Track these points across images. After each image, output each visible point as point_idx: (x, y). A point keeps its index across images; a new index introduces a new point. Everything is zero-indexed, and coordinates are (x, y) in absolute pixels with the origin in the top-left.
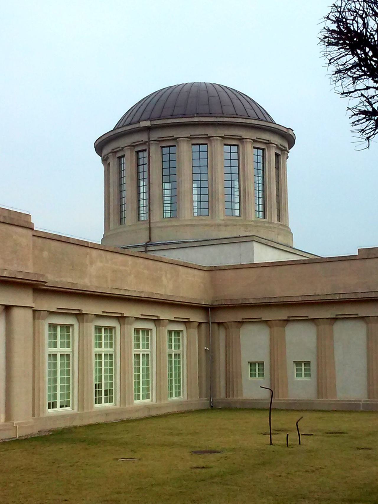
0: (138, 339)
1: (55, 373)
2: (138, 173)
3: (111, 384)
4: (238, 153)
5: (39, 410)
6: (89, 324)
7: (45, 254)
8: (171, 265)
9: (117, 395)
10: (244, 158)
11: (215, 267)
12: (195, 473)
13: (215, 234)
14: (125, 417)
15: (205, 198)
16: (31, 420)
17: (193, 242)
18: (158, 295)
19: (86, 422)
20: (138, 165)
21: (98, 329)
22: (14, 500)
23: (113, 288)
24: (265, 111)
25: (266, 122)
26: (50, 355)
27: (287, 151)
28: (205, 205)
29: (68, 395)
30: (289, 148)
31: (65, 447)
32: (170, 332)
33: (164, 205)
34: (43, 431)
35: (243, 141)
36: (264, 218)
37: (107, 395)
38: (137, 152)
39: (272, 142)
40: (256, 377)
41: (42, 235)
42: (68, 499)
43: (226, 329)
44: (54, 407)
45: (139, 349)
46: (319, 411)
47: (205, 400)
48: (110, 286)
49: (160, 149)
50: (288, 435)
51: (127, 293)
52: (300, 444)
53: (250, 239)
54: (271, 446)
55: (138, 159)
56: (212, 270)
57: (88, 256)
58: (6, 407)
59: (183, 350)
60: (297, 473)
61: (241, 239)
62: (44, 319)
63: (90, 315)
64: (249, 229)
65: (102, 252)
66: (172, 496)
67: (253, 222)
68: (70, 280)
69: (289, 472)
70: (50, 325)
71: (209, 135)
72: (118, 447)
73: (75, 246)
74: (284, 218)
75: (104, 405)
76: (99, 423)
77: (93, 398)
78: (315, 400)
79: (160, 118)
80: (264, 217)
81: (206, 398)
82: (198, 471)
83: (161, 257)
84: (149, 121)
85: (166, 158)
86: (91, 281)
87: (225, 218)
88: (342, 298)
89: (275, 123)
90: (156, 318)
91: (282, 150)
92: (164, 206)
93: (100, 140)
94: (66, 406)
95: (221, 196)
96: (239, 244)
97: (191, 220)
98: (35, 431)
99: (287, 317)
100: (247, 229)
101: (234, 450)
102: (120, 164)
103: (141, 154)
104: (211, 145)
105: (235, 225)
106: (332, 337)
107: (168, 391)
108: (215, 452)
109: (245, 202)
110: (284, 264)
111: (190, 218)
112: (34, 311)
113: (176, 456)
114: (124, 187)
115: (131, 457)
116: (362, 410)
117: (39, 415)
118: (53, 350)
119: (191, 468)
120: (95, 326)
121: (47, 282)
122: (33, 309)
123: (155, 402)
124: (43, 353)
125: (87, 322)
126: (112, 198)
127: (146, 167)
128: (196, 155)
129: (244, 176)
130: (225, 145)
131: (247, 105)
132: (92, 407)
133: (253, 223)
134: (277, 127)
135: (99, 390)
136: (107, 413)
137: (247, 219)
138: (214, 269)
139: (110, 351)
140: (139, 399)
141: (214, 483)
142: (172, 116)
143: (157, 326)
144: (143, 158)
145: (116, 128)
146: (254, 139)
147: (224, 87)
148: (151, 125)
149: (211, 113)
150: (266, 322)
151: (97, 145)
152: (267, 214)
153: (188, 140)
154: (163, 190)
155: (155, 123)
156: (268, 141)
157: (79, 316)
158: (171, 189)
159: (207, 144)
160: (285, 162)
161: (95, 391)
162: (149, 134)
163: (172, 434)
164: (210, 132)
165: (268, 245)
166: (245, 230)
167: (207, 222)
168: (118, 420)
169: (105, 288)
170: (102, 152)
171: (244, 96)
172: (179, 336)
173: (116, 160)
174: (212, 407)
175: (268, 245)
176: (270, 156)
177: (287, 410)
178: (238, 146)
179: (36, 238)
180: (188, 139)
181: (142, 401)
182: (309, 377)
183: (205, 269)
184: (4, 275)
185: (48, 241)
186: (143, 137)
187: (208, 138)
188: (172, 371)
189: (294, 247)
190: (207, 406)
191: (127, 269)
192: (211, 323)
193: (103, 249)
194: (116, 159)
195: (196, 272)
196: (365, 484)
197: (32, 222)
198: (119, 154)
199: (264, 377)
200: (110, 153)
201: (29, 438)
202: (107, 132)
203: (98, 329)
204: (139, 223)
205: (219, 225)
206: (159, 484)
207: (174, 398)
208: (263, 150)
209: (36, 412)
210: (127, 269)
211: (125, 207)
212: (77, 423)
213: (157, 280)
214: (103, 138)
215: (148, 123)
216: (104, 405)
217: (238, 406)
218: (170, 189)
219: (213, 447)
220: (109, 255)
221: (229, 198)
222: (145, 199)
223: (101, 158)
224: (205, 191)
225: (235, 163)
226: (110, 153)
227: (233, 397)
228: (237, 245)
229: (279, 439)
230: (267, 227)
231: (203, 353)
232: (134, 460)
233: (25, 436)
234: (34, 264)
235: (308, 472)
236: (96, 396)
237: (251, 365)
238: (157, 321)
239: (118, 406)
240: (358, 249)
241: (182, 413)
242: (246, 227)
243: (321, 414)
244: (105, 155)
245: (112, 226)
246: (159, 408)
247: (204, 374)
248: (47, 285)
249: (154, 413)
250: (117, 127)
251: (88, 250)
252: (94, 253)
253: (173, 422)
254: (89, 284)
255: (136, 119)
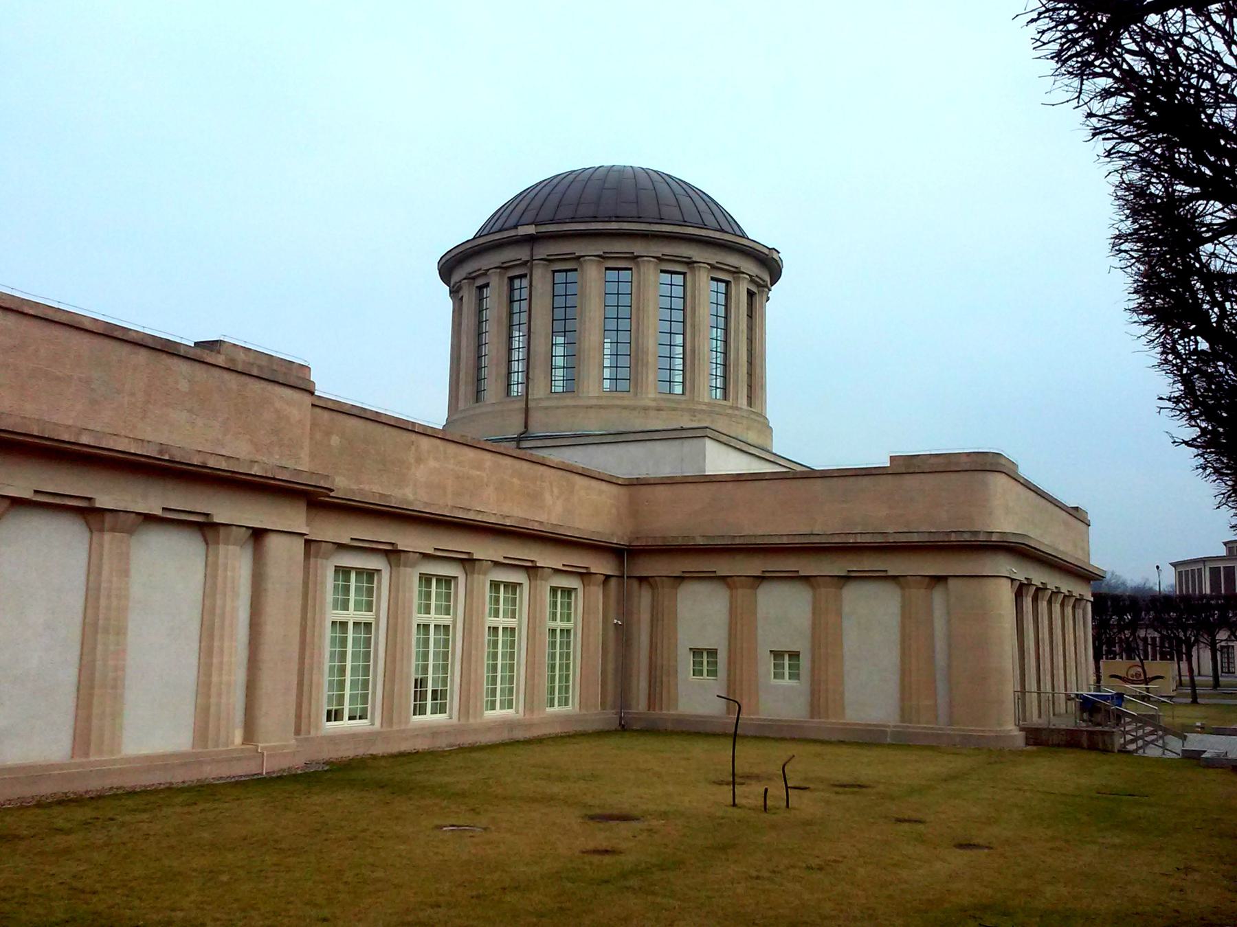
0: (497, 600)
1: (343, 656)
2: (511, 314)
3: (445, 681)
4: (683, 286)
5: (309, 725)
6: (409, 570)
7: (335, 440)
8: (560, 473)
9: (453, 701)
10: (694, 297)
11: (637, 478)
12: (591, 864)
13: (638, 423)
14: (468, 740)
15: (625, 361)
16: (293, 742)
17: (601, 435)
18: (536, 524)
19: (395, 748)
20: (511, 301)
21: (426, 579)
22: (218, 915)
23: (455, 507)
24: (731, 217)
25: (734, 236)
26: (334, 623)
27: (766, 286)
28: (623, 373)
29: (365, 698)
30: (771, 281)
31: (346, 798)
32: (554, 590)
33: (553, 382)
34: (314, 763)
35: (694, 267)
36: (725, 400)
37: (437, 700)
38: (511, 279)
39: (742, 270)
40: (702, 675)
41: (330, 405)
42: (329, 916)
43: (651, 586)
44: (338, 718)
45: (497, 619)
46: (815, 741)
47: (611, 714)
48: (450, 503)
49: (549, 275)
50: (766, 790)
51: (479, 518)
52: (788, 806)
53: (699, 433)
54: (735, 808)
55: (512, 289)
56: (633, 484)
57: (413, 448)
58: (245, 715)
59: (576, 624)
60: (792, 871)
61: (684, 434)
62: (326, 556)
63: (411, 554)
64: (699, 416)
65: (438, 441)
66: (542, 917)
67: (705, 405)
68: (377, 489)
69: (776, 869)
70: (338, 569)
71: (635, 254)
72: (445, 802)
73: (390, 429)
74: (758, 402)
75: (429, 718)
76: (417, 752)
77: (410, 706)
78: (806, 722)
79: (552, 222)
80: (725, 397)
81: (612, 709)
82: (596, 859)
83: (544, 457)
84: (534, 226)
85: (560, 289)
86: (415, 494)
87: (659, 396)
88: (859, 541)
89: (748, 238)
90: (529, 564)
91: (759, 285)
92: (553, 384)
93: (448, 257)
94: (361, 718)
95: (651, 359)
96: (680, 441)
97: (598, 398)
98: (297, 763)
99: (760, 571)
100: (695, 416)
101: (664, 815)
102: (481, 300)
103: (517, 283)
104: (639, 272)
105: (674, 409)
106: (839, 613)
107: (547, 696)
108: (625, 818)
109: (693, 371)
110: (760, 477)
111: (597, 395)
112: (308, 542)
113: (554, 824)
114: (486, 338)
115: (468, 822)
116: (891, 742)
117: (309, 732)
118: (340, 615)
119: (583, 852)
120: (420, 574)
121: (335, 489)
122: (306, 537)
123: (522, 714)
124: (322, 620)
125: (405, 566)
126: (464, 353)
127: (525, 304)
128: (612, 288)
129: (693, 326)
130: (662, 271)
131: (702, 206)
132: (408, 721)
133: (704, 407)
134: (751, 244)
135: (422, 689)
136: (435, 732)
137: (696, 399)
138: (635, 483)
139: (445, 620)
140: (494, 709)
141: (627, 888)
142: (573, 220)
143: (531, 578)
144: (521, 288)
145: (477, 236)
146: (659, 257)
147: (664, 176)
148: (537, 233)
149: (641, 216)
150: (723, 579)
151: (442, 265)
152: (729, 392)
153: (599, 261)
154: (552, 356)
155: (543, 229)
156: (736, 268)
157: (392, 554)
158: (566, 368)
159: (631, 269)
160: (763, 307)
161: (415, 691)
162: (532, 249)
163: (549, 778)
164: (638, 248)
165: (731, 446)
166: (692, 418)
167: (626, 403)
168: (454, 746)
169: (443, 506)
170: (450, 279)
171: (697, 190)
172: (569, 597)
173: (474, 291)
174: (624, 728)
175: (731, 446)
176: (738, 294)
177: (756, 738)
178: (684, 274)
179: (318, 410)
180: (601, 260)
181: (499, 713)
182: (796, 679)
183: (620, 483)
184: (253, 473)
185: (341, 417)
186: (522, 254)
187: (634, 258)
188: (555, 660)
189: (774, 451)
190: (615, 725)
191: (484, 475)
192: (627, 577)
193: (440, 436)
194: (474, 291)
195: (604, 486)
196: (929, 901)
197: (312, 379)
198: (480, 282)
199: (716, 676)
200: (465, 279)
201: (285, 776)
202: (460, 243)
203: (426, 579)
204: (508, 399)
205: (646, 409)
206: (517, 888)
207: (557, 709)
208: (727, 283)
209: (304, 728)
210: (484, 475)
211: (485, 372)
212: (379, 749)
213: (535, 497)
214: (453, 254)
215: (531, 230)
216: (429, 718)
217: (670, 726)
218: (564, 356)
219: (626, 808)
220: (452, 448)
221: (665, 363)
222: (521, 383)
223: (448, 288)
224: (624, 349)
225: (678, 303)
226: (465, 279)
227: (661, 709)
228: (677, 442)
229: (750, 794)
230: (729, 416)
231: (611, 633)
232: (475, 830)
233: (279, 771)
234: (313, 456)
235: (812, 869)
236: (415, 700)
237: (694, 652)
238: (532, 570)
239: (455, 720)
240: (891, 457)
241: (569, 736)
242: (693, 412)
243: (817, 748)
244: (456, 283)
245: (462, 406)
246: (531, 725)
247: (611, 667)
248: (334, 495)
249: (519, 735)
250: (479, 234)
251: (414, 437)
252: (425, 443)
253: (553, 753)
254: (411, 497)
255: (512, 222)
